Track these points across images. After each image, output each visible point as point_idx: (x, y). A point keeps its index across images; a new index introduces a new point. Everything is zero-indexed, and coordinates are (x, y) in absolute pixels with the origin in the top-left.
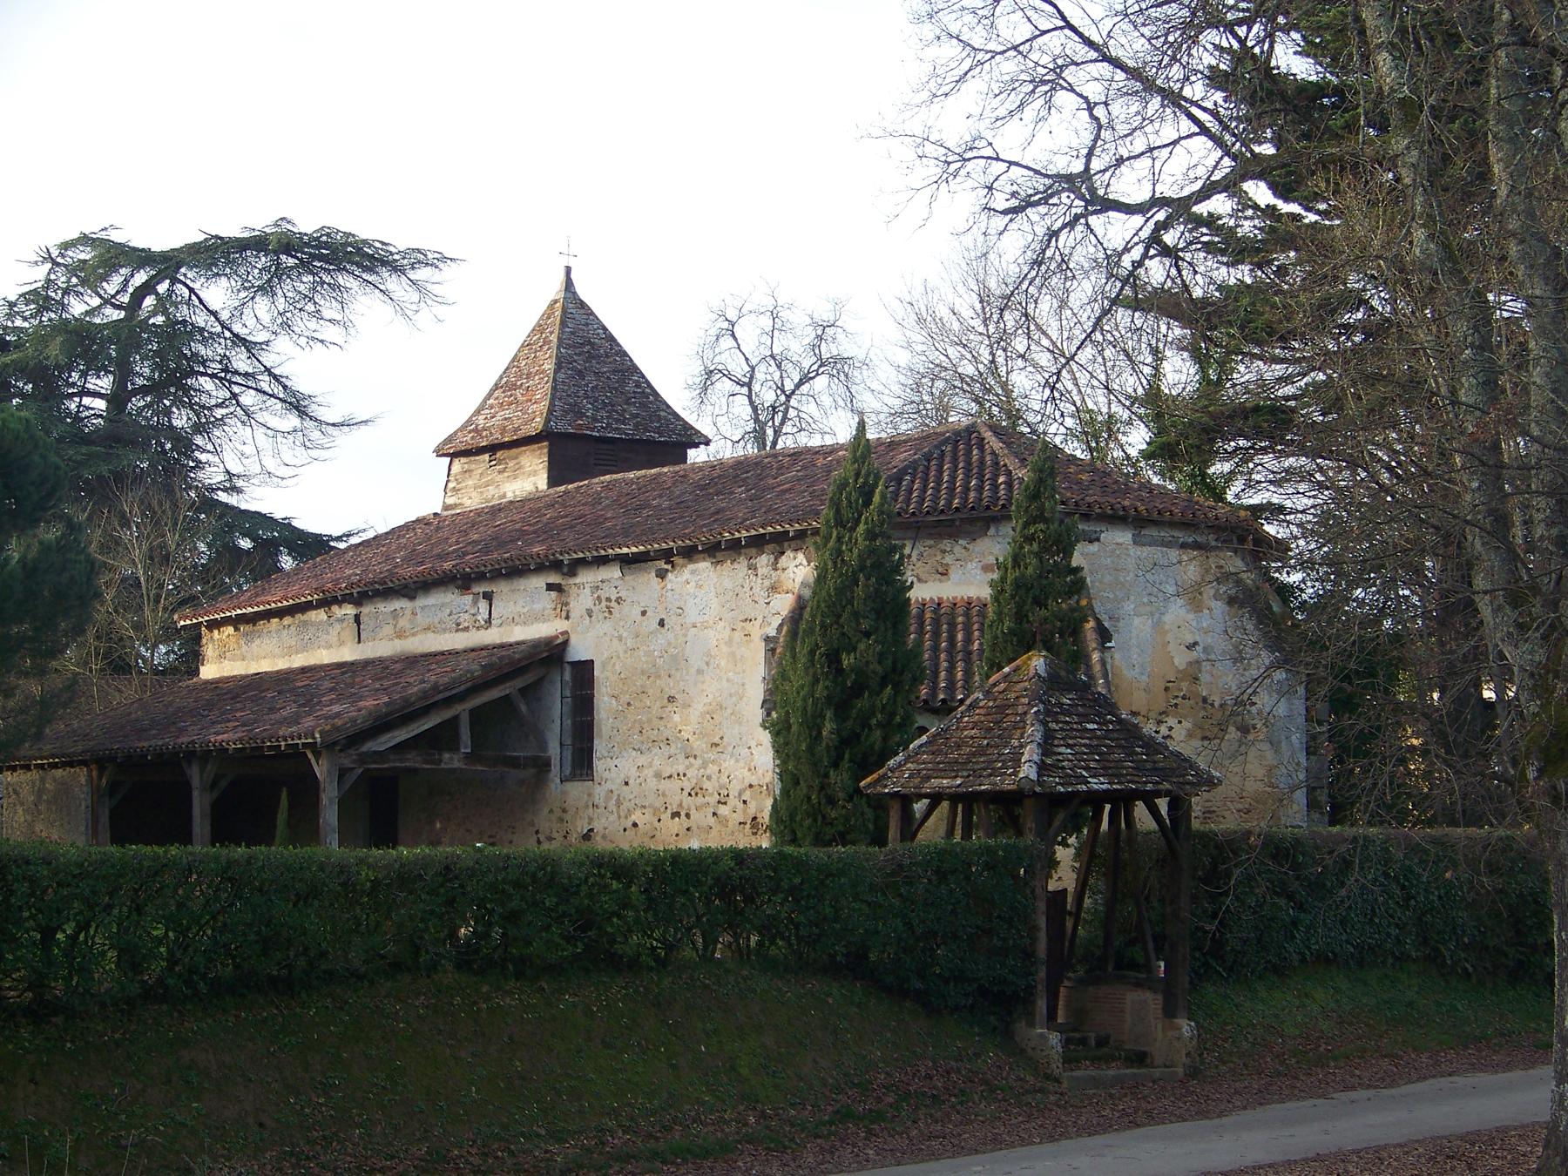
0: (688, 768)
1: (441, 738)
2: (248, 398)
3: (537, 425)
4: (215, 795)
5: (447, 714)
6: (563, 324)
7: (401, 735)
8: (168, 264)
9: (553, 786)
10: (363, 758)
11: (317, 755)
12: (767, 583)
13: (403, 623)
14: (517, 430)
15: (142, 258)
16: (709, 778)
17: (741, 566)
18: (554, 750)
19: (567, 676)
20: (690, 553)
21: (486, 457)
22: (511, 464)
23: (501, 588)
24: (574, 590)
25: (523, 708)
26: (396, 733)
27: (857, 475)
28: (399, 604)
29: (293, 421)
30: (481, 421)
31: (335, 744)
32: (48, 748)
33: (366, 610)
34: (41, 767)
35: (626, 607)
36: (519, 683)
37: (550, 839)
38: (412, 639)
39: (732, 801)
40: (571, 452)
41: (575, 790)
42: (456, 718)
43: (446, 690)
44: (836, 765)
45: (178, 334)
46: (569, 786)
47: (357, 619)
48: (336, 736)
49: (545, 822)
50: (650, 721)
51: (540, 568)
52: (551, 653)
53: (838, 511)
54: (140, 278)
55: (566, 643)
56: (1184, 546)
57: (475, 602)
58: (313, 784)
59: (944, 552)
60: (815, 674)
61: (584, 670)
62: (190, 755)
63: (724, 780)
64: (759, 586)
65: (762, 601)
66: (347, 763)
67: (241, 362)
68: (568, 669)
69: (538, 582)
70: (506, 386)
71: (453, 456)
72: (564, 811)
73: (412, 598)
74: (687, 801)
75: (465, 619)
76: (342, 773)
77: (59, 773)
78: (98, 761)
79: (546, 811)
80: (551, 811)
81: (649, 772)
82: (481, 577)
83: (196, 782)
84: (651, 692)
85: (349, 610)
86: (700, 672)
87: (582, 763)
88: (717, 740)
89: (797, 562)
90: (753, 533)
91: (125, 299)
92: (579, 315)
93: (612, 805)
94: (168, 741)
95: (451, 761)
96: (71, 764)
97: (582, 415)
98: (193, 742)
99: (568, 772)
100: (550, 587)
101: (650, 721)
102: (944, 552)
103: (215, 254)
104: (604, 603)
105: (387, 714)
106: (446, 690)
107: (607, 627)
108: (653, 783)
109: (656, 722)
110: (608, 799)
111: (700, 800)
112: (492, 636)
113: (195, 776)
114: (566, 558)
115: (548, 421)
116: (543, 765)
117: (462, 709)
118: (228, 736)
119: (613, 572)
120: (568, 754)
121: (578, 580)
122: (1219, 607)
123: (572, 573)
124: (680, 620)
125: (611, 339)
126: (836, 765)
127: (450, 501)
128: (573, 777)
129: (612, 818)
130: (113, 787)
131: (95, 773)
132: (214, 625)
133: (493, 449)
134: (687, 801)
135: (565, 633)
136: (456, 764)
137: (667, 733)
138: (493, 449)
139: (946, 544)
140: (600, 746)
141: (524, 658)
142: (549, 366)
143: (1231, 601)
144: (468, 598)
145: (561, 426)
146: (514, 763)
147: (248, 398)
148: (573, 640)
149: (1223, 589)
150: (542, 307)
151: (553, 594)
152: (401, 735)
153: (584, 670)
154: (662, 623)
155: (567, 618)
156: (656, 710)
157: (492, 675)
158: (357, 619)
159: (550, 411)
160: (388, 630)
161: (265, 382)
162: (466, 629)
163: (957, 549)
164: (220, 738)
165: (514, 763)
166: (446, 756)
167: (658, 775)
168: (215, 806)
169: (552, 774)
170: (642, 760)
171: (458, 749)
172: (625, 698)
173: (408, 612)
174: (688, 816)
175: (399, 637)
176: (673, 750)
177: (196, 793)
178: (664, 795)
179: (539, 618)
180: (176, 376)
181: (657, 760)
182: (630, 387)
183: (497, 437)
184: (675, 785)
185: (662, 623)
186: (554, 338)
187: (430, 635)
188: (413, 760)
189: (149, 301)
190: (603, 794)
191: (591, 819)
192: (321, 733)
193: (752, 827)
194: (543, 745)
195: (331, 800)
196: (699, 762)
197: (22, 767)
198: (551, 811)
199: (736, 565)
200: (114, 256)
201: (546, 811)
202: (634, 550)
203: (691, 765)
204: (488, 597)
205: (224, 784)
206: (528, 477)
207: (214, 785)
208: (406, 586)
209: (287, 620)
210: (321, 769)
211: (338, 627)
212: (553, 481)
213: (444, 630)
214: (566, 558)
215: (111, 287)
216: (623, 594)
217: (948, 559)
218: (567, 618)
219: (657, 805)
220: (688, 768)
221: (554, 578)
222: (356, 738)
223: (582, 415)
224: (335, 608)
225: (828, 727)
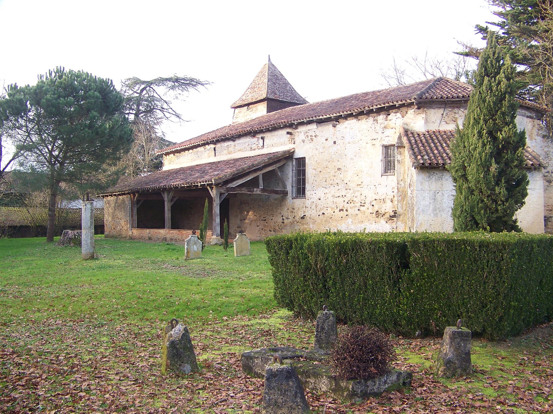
0: (346, 193)
1: (254, 183)
2: (167, 115)
3: (264, 96)
4: (173, 203)
5: (255, 175)
6: (269, 70)
7: (240, 182)
8: (149, 84)
9: (289, 201)
10: (228, 190)
11: (212, 188)
12: (383, 126)
13: (231, 149)
14: (256, 99)
15: (143, 82)
16: (356, 197)
17: (371, 119)
18: (289, 188)
19: (294, 163)
20: (346, 117)
21: (246, 107)
22: (254, 109)
23: (267, 136)
24: (297, 134)
25: (279, 174)
26: (239, 181)
27: (494, 53)
28: (230, 143)
29: (178, 119)
30: (244, 98)
31: (219, 184)
32: (117, 190)
33: (218, 146)
34: (115, 195)
35: (318, 138)
36: (278, 165)
37: (288, 218)
38: (234, 154)
39: (367, 205)
40: (273, 104)
41: (298, 202)
42: (258, 176)
43: (256, 166)
44: (497, 184)
45: (151, 99)
46: (295, 200)
47: (215, 149)
48: (220, 181)
49: (285, 212)
50: (330, 177)
51: (285, 127)
52: (288, 156)
53: (486, 69)
54: (143, 86)
55: (294, 152)
56: (527, 117)
57: (258, 141)
58: (211, 200)
59: (455, 113)
60: (483, 142)
61: (301, 162)
62: (165, 189)
63: (363, 197)
64: (378, 127)
65: (380, 132)
66: (223, 191)
67: (165, 106)
68: (294, 160)
69: (283, 132)
70: (252, 88)
71: (235, 108)
72: (293, 209)
73: (234, 141)
74: (346, 206)
75: (254, 146)
76: (221, 194)
77: (121, 197)
78: (133, 192)
79: (286, 209)
80: (288, 209)
81: (329, 195)
82: (261, 132)
83: (166, 199)
84: (330, 167)
85: (212, 146)
86: (351, 159)
87: (301, 191)
88: (360, 183)
89: (397, 117)
90: (379, 106)
91: (139, 91)
92: (273, 68)
93: (314, 207)
94: (157, 185)
95: (257, 191)
96: (124, 194)
97: (276, 94)
98: (166, 185)
99: (294, 196)
100: (288, 133)
101: (330, 177)
102: (455, 113)
103: (161, 81)
104: (310, 137)
105: (237, 174)
106: (256, 166)
107: (311, 145)
108: (331, 199)
109: (332, 178)
110: (311, 205)
111: (352, 205)
112: (265, 151)
113: (166, 197)
114: (296, 122)
115: (267, 95)
116: (285, 193)
117: (260, 173)
118: (177, 182)
119: (313, 126)
120: (294, 190)
121: (298, 130)
122: (539, 139)
123: (296, 128)
124: (343, 141)
125: (282, 75)
126: (497, 184)
127: (234, 121)
128: (296, 197)
129: (313, 211)
130: (138, 201)
131: (132, 197)
132: (167, 154)
133: (248, 105)
134: (346, 206)
135: (294, 148)
136: (258, 192)
137: (337, 181)
138: (248, 105)
139: (456, 110)
140: (308, 186)
141: (281, 156)
142: (266, 81)
143: (544, 137)
144: (255, 139)
145: (271, 97)
146: (277, 192)
147: (167, 115)
148: (297, 151)
149: (540, 132)
150: (262, 66)
151: (289, 135)
152: (240, 182)
153: (301, 162)
154: (335, 143)
155: (294, 143)
156: (332, 173)
157: (271, 161)
158: (215, 149)
159: (267, 92)
160: (226, 152)
161: (170, 111)
162: (254, 149)
163: (460, 112)
164: (175, 183)
165: (277, 192)
166: (255, 189)
167: (333, 196)
168: (172, 207)
169: (288, 197)
170: (326, 191)
171: (258, 187)
172: (320, 170)
173: (232, 146)
174: (347, 210)
175: (229, 154)
176: (340, 187)
177: (166, 203)
178: (336, 203)
179: (284, 144)
180: (150, 111)
181: (333, 191)
182: (288, 88)
183: (250, 101)
184: (341, 199)
185: (335, 143)
186: (267, 74)
187: (241, 152)
188: (244, 191)
189: (145, 92)
190: (310, 203)
191: (304, 212)
192: (215, 180)
193: (376, 215)
194: (285, 186)
195: (217, 205)
196: (352, 191)
197: (110, 195)
198: (288, 209)
199: (368, 120)
200: (137, 82)
201: (286, 209)
202: (325, 117)
203: (348, 192)
204: (263, 138)
205: (175, 200)
206: (261, 110)
207: (172, 201)
208: (233, 137)
209: (191, 151)
210: (213, 193)
211: (208, 152)
212: (268, 112)
213: (246, 151)
214: (296, 122)
215: (136, 88)
216: (317, 134)
217: (457, 116)
218: (294, 143)
219: (333, 207)
220: (346, 193)
221: (289, 130)
222: (227, 182)
223: (276, 94)
224: (207, 146)
225: (494, 168)
